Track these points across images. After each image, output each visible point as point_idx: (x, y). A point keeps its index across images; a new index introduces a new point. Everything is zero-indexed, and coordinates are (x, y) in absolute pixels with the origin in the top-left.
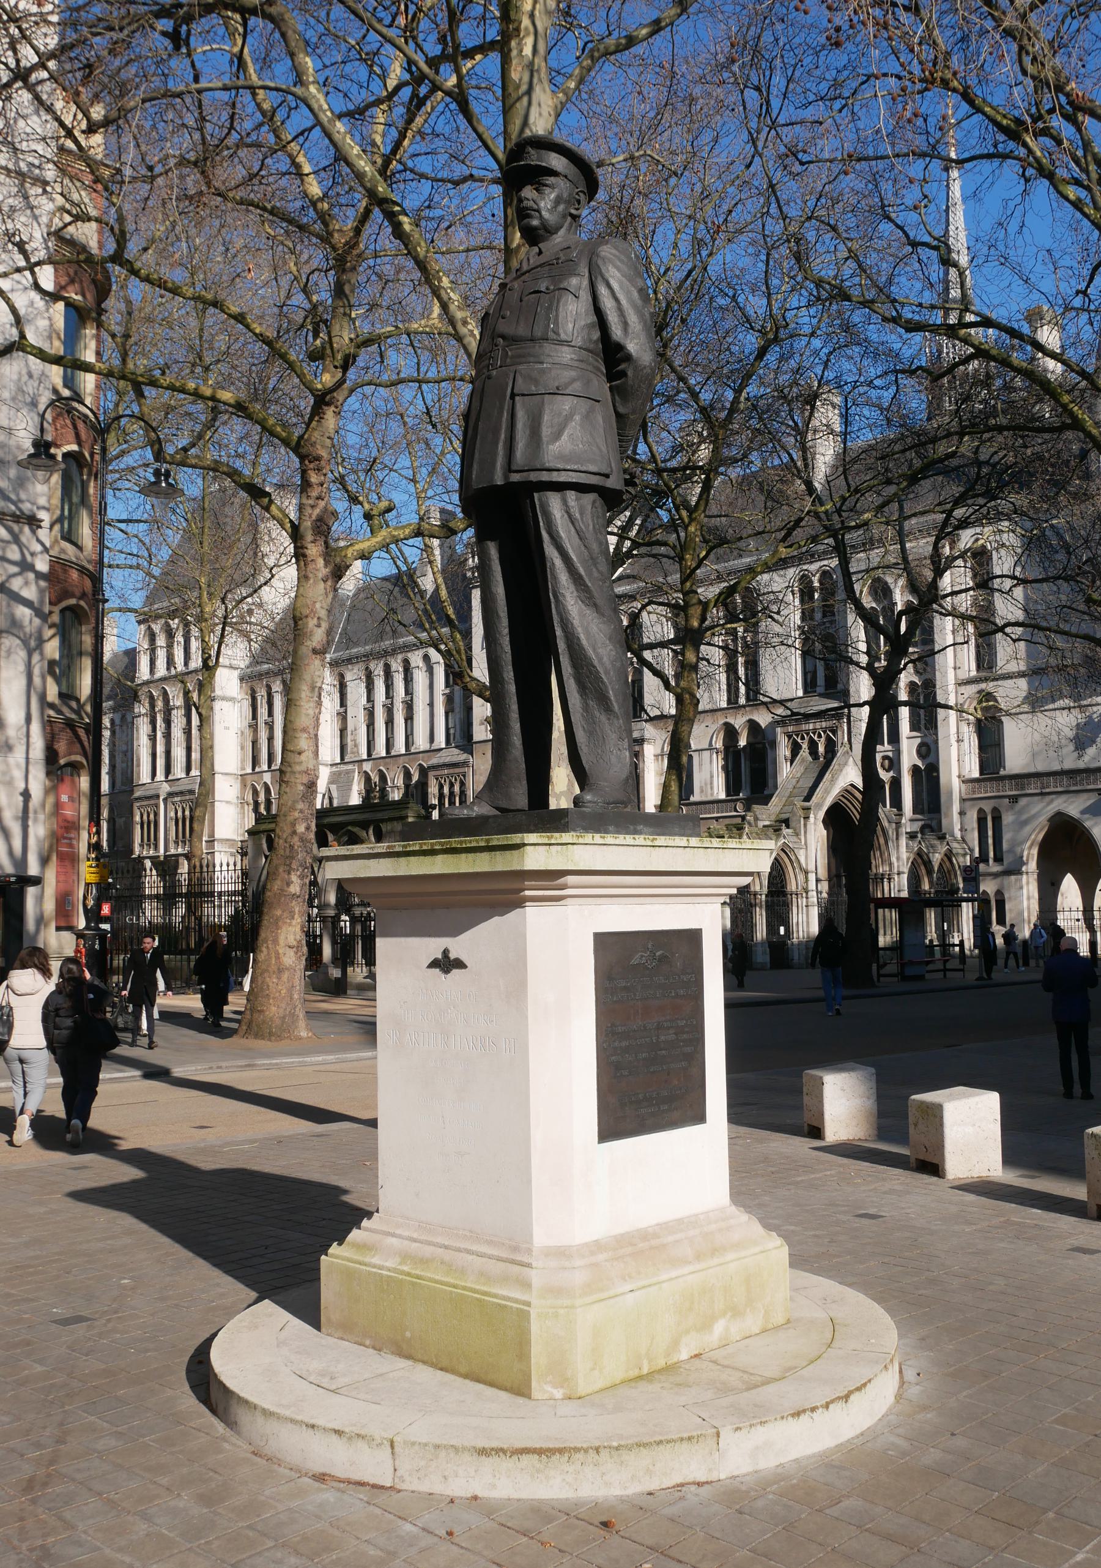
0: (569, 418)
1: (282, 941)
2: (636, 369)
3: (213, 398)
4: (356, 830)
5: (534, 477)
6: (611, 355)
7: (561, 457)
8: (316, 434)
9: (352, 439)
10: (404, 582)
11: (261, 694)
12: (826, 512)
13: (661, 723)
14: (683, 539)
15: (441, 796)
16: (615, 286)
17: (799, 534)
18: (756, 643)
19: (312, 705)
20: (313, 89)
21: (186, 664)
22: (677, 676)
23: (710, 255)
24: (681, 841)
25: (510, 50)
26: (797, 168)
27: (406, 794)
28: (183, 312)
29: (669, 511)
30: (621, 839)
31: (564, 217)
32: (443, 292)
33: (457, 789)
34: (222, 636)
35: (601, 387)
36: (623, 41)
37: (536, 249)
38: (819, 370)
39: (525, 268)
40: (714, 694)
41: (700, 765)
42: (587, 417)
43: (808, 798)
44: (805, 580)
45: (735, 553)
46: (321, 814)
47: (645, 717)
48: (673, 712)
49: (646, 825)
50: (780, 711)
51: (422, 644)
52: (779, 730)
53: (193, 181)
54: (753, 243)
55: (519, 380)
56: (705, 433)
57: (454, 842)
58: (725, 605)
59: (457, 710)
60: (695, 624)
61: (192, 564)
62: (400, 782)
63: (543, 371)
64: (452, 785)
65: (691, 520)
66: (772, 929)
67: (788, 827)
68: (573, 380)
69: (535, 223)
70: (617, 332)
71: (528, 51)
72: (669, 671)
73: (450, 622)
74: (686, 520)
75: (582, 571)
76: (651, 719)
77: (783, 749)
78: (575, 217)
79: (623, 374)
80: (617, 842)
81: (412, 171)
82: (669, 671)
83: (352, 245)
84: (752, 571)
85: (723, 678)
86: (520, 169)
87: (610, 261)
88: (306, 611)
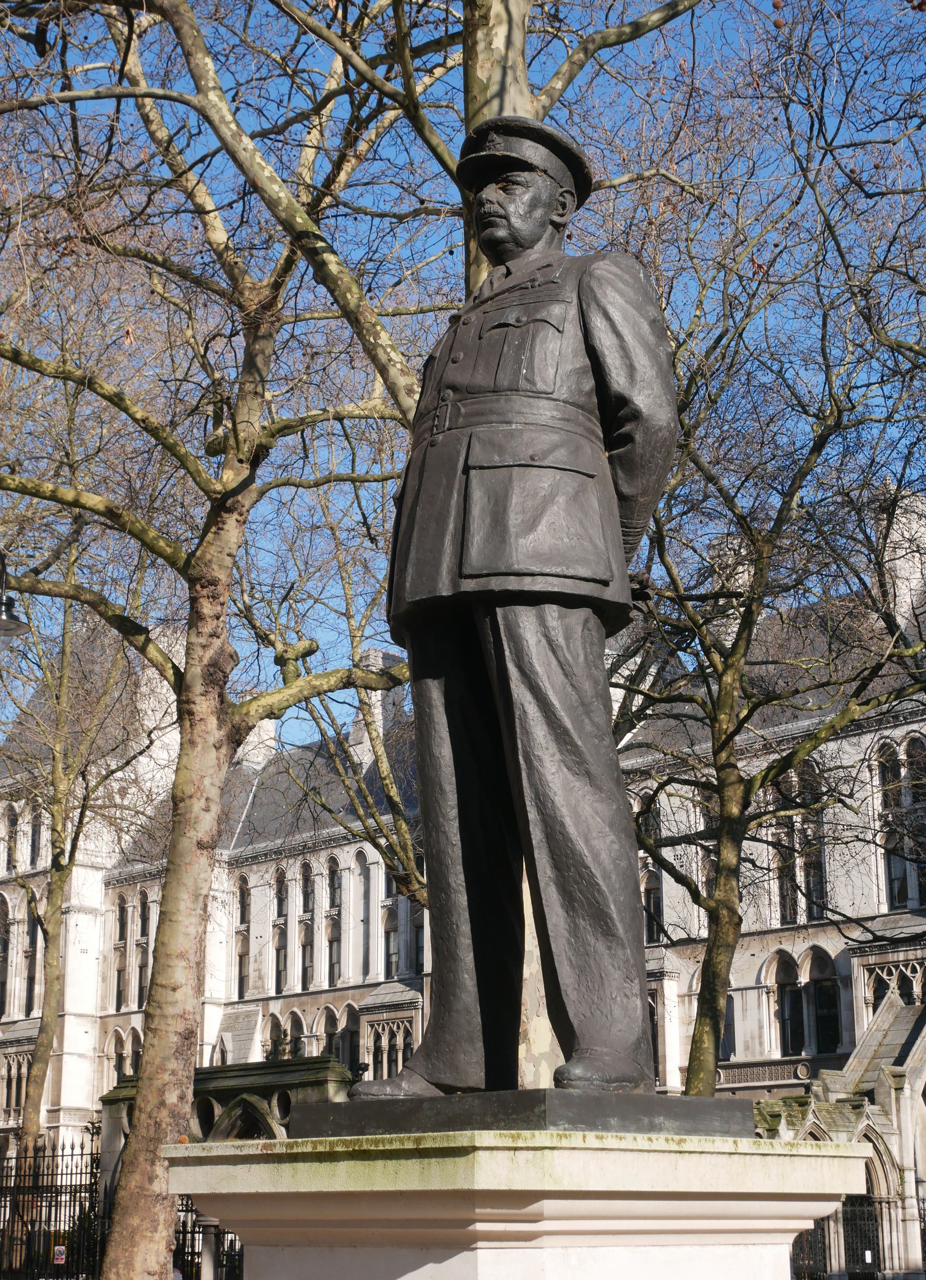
0: (548, 500)
1: (138, 1265)
2: (647, 431)
3: (76, 503)
4: (254, 1099)
5: (496, 584)
6: (612, 413)
7: (537, 556)
8: (213, 550)
9: (265, 560)
10: (332, 751)
11: (133, 903)
12: (914, 657)
13: (688, 950)
14: (715, 695)
15: (378, 1051)
16: (616, 316)
17: (876, 686)
18: (820, 838)
19: (194, 920)
20: (213, 96)
21: (33, 862)
22: (711, 884)
23: (747, 315)
24: (724, 1143)
25: (475, 43)
26: (863, 203)
27: (329, 1048)
28: (50, 399)
29: (697, 655)
30: (631, 1140)
31: (543, 225)
32: (380, 352)
33: (400, 1040)
34: (81, 821)
35: (596, 457)
36: (627, 30)
37: (502, 269)
38: (898, 467)
39: (487, 293)
40: (761, 909)
41: (744, 1010)
42: (576, 498)
43: (900, 1060)
44: (886, 750)
45: (789, 713)
46: (202, 1076)
47: (665, 941)
48: (704, 934)
50: (857, 934)
51: (352, 837)
52: (855, 961)
53: (56, 222)
54: (804, 301)
55: (477, 448)
56: (743, 552)
57: (366, 1141)
58: (776, 784)
59: (401, 928)
60: (735, 810)
61: (45, 726)
62: (320, 1029)
63: (511, 434)
64: (393, 1035)
65: (727, 667)
66: (854, 1255)
67: (872, 1102)
68: (555, 447)
69: (501, 233)
70: (618, 380)
71: (499, 42)
72: (699, 878)
73: (393, 807)
74: (720, 667)
75: (568, 723)
76: (673, 944)
77: (862, 989)
78: (558, 227)
79: (628, 439)
80: (623, 1145)
81: (345, 205)
82: (699, 878)
83: (268, 305)
84: (812, 737)
85: (775, 886)
86: (483, 165)
87: (609, 282)
88: (190, 790)
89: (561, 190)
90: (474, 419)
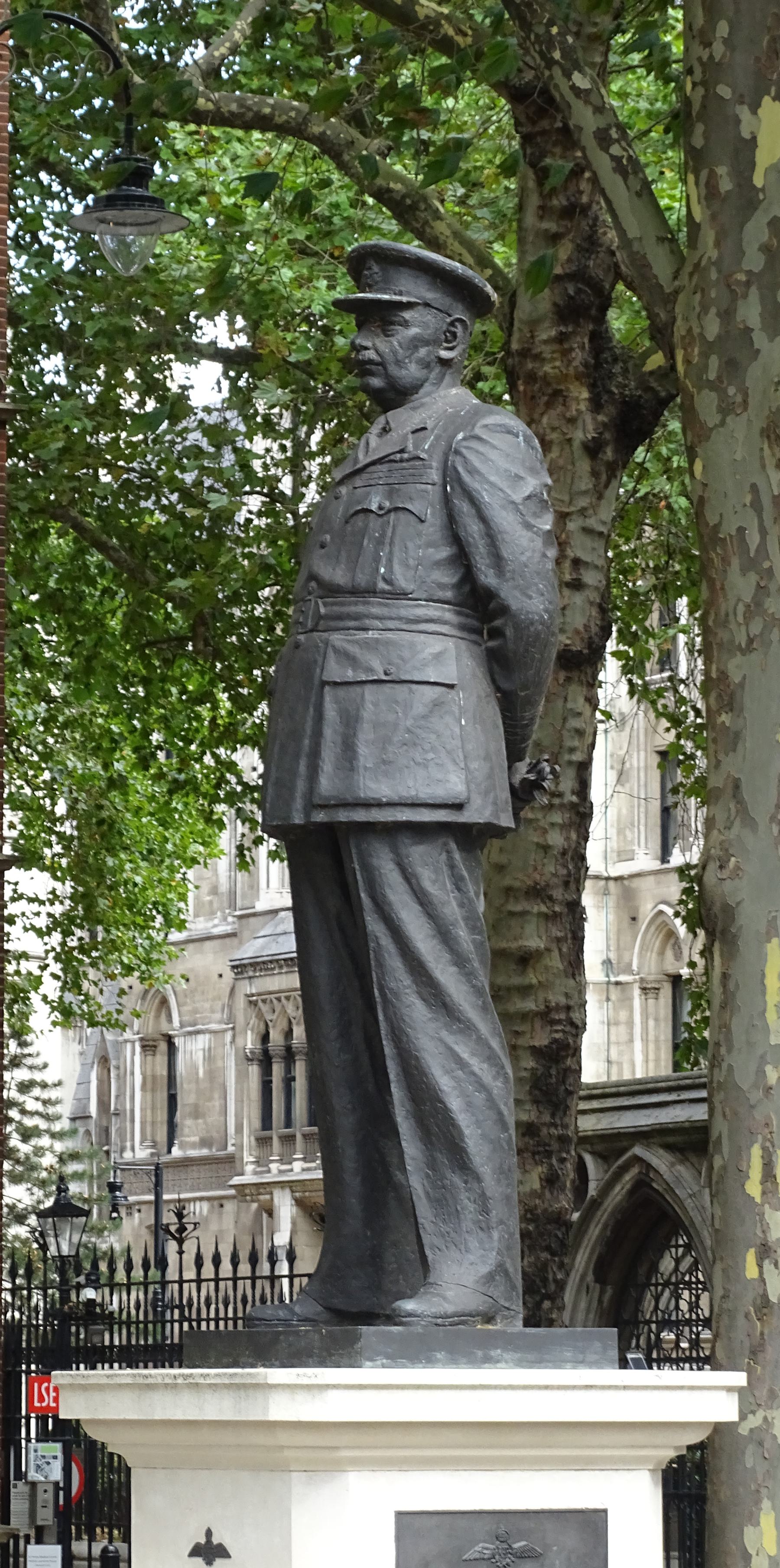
2: (517, 627)
49: (505, 1349)
89: (449, 320)
90: (333, 624)
